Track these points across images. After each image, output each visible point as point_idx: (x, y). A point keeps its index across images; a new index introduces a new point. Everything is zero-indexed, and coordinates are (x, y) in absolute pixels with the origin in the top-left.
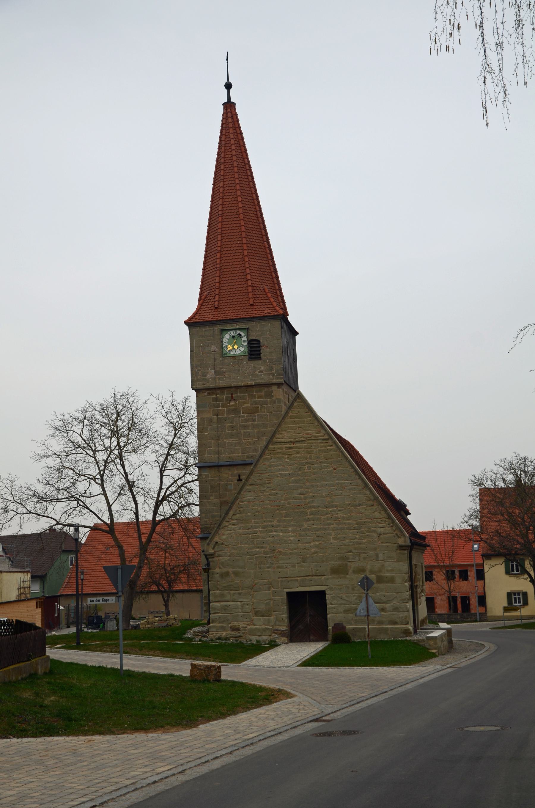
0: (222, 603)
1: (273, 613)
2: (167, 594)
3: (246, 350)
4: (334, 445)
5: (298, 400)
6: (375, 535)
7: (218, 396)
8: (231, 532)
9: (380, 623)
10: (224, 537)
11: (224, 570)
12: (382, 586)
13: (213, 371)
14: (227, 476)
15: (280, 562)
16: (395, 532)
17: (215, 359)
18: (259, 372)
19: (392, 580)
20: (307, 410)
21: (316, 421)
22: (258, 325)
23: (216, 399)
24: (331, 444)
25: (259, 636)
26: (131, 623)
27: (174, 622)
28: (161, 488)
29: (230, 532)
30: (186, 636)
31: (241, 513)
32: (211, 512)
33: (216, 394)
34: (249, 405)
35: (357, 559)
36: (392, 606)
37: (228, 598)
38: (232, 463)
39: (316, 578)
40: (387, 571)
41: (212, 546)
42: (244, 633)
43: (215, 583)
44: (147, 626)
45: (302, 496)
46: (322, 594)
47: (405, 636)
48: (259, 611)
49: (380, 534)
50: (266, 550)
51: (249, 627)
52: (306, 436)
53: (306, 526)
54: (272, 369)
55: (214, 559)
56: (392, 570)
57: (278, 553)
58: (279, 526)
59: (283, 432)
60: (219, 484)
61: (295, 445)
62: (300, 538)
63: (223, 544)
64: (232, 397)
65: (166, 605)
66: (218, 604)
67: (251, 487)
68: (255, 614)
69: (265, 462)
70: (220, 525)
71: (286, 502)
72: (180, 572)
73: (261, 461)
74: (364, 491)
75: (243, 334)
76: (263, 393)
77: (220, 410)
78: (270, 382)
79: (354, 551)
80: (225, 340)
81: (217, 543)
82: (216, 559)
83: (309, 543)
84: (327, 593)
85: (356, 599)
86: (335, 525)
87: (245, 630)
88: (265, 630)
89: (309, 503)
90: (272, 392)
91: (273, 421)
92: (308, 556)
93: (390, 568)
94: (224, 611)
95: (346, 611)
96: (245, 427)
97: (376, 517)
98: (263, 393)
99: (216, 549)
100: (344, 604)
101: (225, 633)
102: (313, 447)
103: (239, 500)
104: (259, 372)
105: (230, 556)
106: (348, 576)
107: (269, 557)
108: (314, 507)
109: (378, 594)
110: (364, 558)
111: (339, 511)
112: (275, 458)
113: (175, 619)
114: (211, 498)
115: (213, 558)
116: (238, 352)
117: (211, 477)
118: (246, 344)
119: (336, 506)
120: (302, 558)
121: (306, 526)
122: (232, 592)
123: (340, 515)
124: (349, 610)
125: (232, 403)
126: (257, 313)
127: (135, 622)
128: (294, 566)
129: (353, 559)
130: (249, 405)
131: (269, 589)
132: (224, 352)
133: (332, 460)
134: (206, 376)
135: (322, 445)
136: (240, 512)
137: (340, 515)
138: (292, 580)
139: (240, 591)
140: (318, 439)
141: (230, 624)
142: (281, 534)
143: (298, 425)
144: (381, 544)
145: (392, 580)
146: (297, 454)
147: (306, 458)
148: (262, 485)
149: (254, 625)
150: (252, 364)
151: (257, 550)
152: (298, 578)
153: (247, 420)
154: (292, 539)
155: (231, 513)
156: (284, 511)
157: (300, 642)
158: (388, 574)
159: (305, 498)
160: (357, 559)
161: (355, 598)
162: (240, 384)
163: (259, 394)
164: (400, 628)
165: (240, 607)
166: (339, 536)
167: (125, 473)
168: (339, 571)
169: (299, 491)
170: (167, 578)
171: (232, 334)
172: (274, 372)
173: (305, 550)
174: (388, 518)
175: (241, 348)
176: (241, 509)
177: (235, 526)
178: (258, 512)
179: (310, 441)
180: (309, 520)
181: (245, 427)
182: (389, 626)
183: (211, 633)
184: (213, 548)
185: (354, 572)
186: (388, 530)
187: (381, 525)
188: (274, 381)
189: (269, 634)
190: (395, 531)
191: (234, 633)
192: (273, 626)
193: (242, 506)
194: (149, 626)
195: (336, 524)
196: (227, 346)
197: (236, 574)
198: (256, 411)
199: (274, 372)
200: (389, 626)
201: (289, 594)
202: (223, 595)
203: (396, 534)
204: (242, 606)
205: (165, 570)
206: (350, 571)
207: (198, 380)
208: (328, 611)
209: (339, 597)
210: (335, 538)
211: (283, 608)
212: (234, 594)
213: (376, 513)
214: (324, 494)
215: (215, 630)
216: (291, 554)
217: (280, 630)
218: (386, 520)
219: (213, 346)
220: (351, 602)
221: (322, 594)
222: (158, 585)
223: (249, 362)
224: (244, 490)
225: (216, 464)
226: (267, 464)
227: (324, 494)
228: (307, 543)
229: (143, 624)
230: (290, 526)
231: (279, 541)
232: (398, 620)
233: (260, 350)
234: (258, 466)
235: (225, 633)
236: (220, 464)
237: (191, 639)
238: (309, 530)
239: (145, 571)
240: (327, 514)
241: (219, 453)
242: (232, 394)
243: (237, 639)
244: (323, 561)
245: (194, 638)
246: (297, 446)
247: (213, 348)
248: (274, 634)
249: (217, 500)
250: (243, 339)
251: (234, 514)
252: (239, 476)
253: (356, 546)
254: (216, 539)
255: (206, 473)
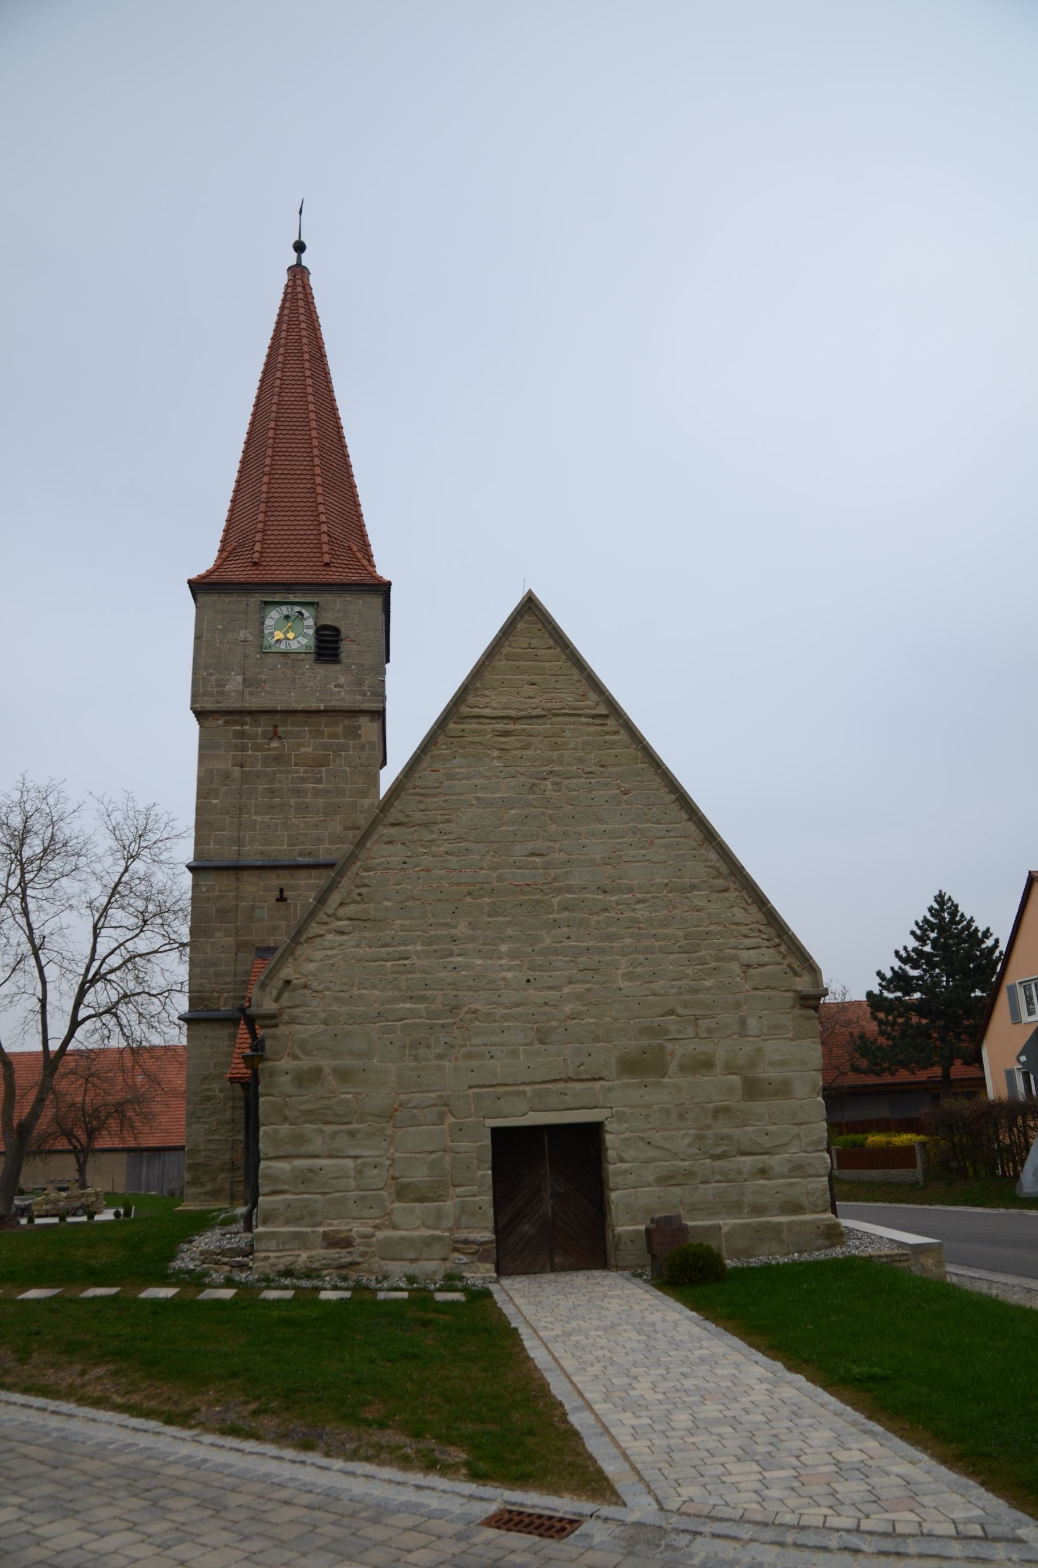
0: (297, 1162)
1: (452, 1190)
2: (83, 1154)
3: (312, 643)
4: (622, 732)
5: (526, 617)
6: (735, 967)
7: (247, 727)
8: (333, 952)
9: (758, 1209)
10: (311, 967)
11: (306, 1063)
12: (759, 1106)
13: (240, 678)
14: (255, 889)
15: (476, 1040)
16: (787, 961)
17: (246, 656)
18: (336, 686)
19: (784, 1090)
20: (551, 642)
21: (575, 671)
22: (339, 600)
23: (242, 735)
24: (615, 729)
25: (412, 1261)
26: (16, 1202)
27: (94, 1199)
28: (92, 959)
29: (329, 953)
30: (177, 1264)
31: (363, 901)
32: (215, 965)
33: (243, 725)
34: (310, 750)
35: (690, 1032)
36: (789, 1161)
37: (317, 1145)
38: (266, 863)
39: (578, 1086)
40: (772, 1064)
41: (275, 993)
42: (364, 1254)
43: (279, 1100)
44: (44, 1207)
45: (537, 859)
46: (593, 1132)
47: (827, 1243)
48: (408, 1185)
49: (748, 966)
50: (433, 1007)
51: (380, 1235)
52: (549, 705)
53: (548, 941)
54: (361, 683)
55: (277, 1031)
56: (784, 1063)
57: (470, 1016)
58: (473, 939)
59: (487, 693)
60: (237, 906)
61: (517, 727)
62: (531, 975)
63: (305, 986)
64: (275, 732)
65: (81, 1171)
66: (284, 1165)
67: (393, 831)
68: (397, 1193)
69: (436, 766)
70: (299, 933)
71: (494, 875)
72: (109, 1115)
73: (425, 763)
74: (703, 851)
75: (306, 614)
76: (340, 729)
77: (249, 756)
78: (357, 706)
79: (681, 1011)
80: (268, 622)
81: (288, 982)
82: (283, 1030)
83: (558, 988)
84: (608, 1128)
85: (690, 1145)
86: (628, 941)
87: (368, 1245)
88: (429, 1242)
89: (556, 879)
90: (359, 727)
91: (357, 784)
92: (554, 1023)
93: (777, 1057)
94: (301, 1188)
95: (663, 1180)
96: (299, 793)
97: (735, 919)
98: (340, 729)
99: (284, 1001)
100: (657, 1160)
101: (305, 1255)
102: (567, 734)
103: (359, 864)
104: (333, 685)
105: (325, 1022)
106: (664, 1080)
107: (443, 1026)
108: (569, 890)
109: (749, 1129)
110: (710, 1030)
111: (639, 901)
112: (465, 757)
113: (97, 1194)
114: (218, 934)
115: (276, 1026)
116: (294, 646)
117: (220, 891)
118: (311, 632)
119: (631, 890)
120: (538, 1031)
121: (548, 941)
122: (329, 1129)
123: (642, 912)
124: (671, 1177)
125: (275, 744)
126: (335, 578)
127: (23, 1200)
128: (514, 1054)
129: (679, 1032)
130: (310, 750)
131: (441, 1118)
132: (266, 643)
133: (618, 769)
134: (224, 686)
135: (592, 729)
136: (362, 899)
137: (642, 912)
138: (507, 1094)
139: (355, 1126)
140: (579, 715)
141: (320, 1224)
142: (479, 962)
143: (526, 677)
144: (752, 993)
145: (784, 1090)
146: (523, 748)
147: (551, 761)
148: (426, 825)
149: (394, 1227)
150: (322, 670)
151: (408, 1006)
152: (527, 1088)
153: (303, 780)
154: (509, 975)
155: (335, 898)
156: (487, 900)
157: (525, 1273)
158: (772, 1074)
159: (547, 866)
160: (690, 1032)
161: (687, 1141)
162: (295, 706)
163: (331, 729)
164: (810, 1222)
165: (352, 1173)
166: (639, 969)
167: (29, 925)
168: (642, 1066)
169: (530, 846)
170: (86, 1124)
171: (285, 613)
172: (366, 688)
173: (546, 1009)
174: (769, 924)
175: (300, 639)
176: (364, 891)
177: (345, 937)
178: (412, 898)
179: (559, 719)
180: (556, 924)
181: (299, 793)
182: (783, 1219)
183: (263, 1255)
184: (277, 999)
185: (682, 1068)
186: (768, 954)
187: (748, 942)
188: (366, 706)
189: (442, 1254)
190: (784, 958)
191: (333, 1253)
192: (450, 1229)
193: (367, 881)
194: (48, 1207)
195: (631, 936)
196: (272, 633)
197: (344, 1075)
198: (323, 762)
199: (366, 688)
200: (783, 1219)
201: (496, 1131)
202: (299, 1139)
203: (789, 966)
204: (359, 1171)
205: (83, 1110)
206: (673, 1067)
207: (206, 694)
208: (612, 1180)
209: (642, 1139)
210: (629, 976)
211: (483, 1176)
212: (335, 1133)
213: (735, 910)
214: (598, 857)
215: (273, 1245)
216: (506, 1018)
217: (474, 1242)
218: (763, 928)
219: (243, 631)
220: (676, 1154)
221: (593, 1132)
222: (69, 1135)
223: (316, 666)
224: (375, 837)
225: (234, 864)
226: (442, 771)
227: (598, 857)
228: (551, 988)
229: (38, 1203)
230: (503, 940)
231: (471, 982)
232: (804, 1201)
233: (337, 648)
234: (417, 775)
235: (305, 1255)
236: (240, 864)
237: (196, 1280)
238: (556, 952)
239: (48, 1113)
240: (606, 910)
241: (239, 842)
242: (275, 726)
243: (344, 1272)
244: (597, 1039)
245: (206, 1274)
246: (524, 730)
247: (242, 634)
248: (456, 1255)
249: (230, 940)
250: (306, 623)
251: (341, 904)
252: (281, 891)
253: (687, 997)
254: (287, 972)
255: (210, 880)
